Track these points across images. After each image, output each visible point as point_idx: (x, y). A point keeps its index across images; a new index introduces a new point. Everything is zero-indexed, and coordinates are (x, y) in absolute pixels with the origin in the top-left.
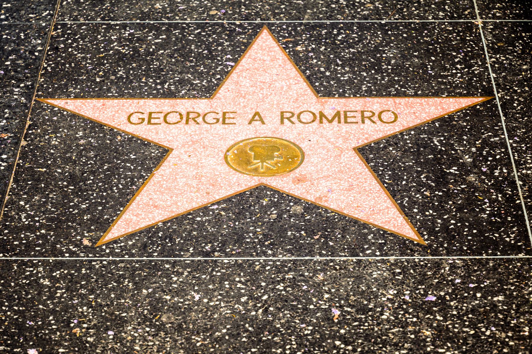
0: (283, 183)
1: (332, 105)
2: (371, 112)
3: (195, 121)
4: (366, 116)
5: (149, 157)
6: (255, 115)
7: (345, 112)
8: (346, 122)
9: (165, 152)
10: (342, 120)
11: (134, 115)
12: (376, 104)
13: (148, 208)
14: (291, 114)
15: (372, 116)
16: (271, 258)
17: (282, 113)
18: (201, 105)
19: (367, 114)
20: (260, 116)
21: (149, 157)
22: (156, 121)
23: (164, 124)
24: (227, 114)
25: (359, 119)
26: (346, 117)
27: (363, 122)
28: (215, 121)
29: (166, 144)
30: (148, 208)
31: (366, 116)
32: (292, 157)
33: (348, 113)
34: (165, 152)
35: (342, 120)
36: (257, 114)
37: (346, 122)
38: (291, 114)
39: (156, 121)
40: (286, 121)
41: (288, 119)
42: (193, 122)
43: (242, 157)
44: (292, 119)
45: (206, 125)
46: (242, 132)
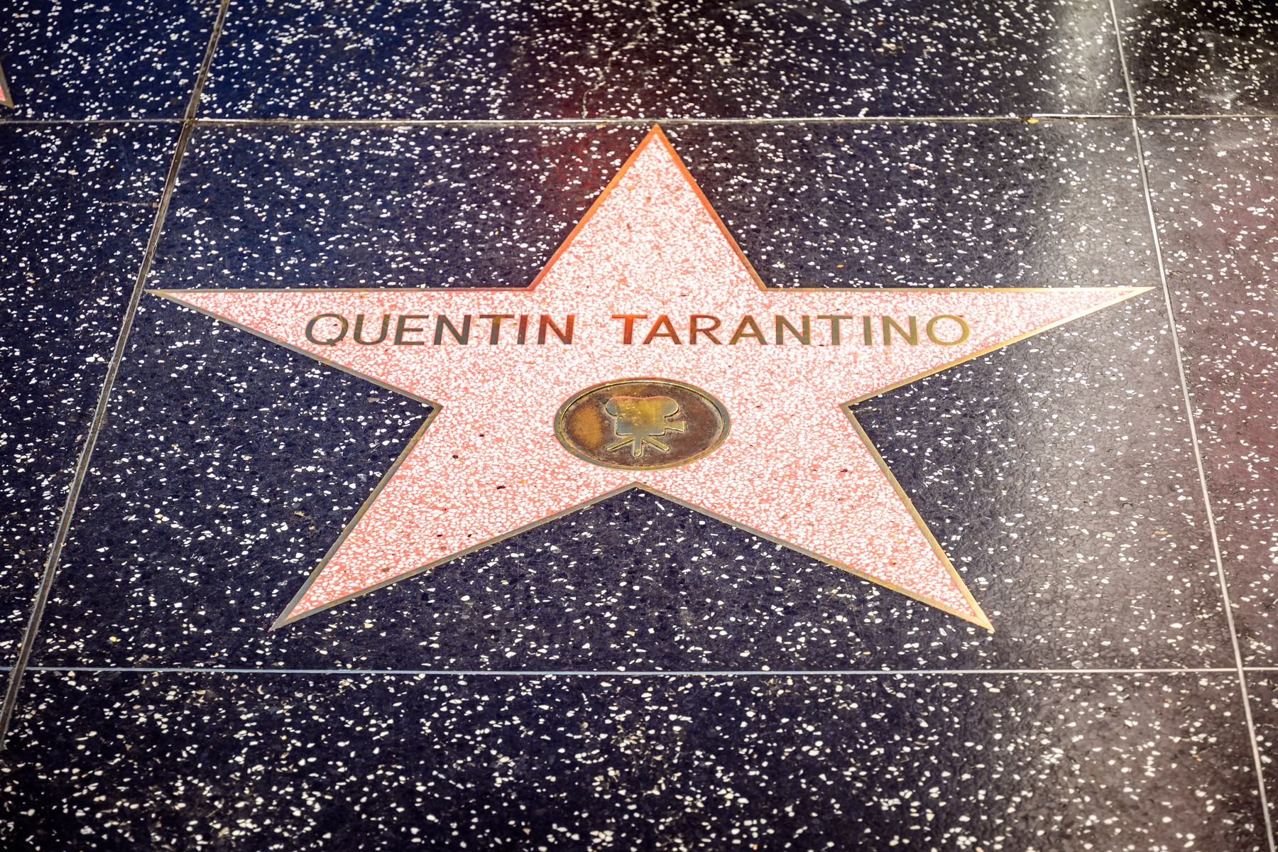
0: (684, 484)
2: (712, 318)
3: (709, 336)
4: (699, 327)
5: (377, 426)
6: (742, 326)
8: (398, 341)
9: (422, 412)
11: (319, 323)
13: (392, 538)
14: (712, 323)
15: (713, 328)
16: (946, 671)
17: (694, 319)
19: (704, 324)
20: (754, 327)
21: (377, 426)
22: (414, 337)
24: (408, 321)
25: (429, 334)
26: (401, 330)
30: (392, 538)
31: (699, 327)
32: (700, 424)
34: (422, 412)
36: (748, 320)
37: (398, 341)
38: (712, 323)
39: (414, 337)
40: (701, 338)
41: (707, 332)
43: (587, 422)
44: (714, 333)
45: (933, 347)
46: (600, 360)
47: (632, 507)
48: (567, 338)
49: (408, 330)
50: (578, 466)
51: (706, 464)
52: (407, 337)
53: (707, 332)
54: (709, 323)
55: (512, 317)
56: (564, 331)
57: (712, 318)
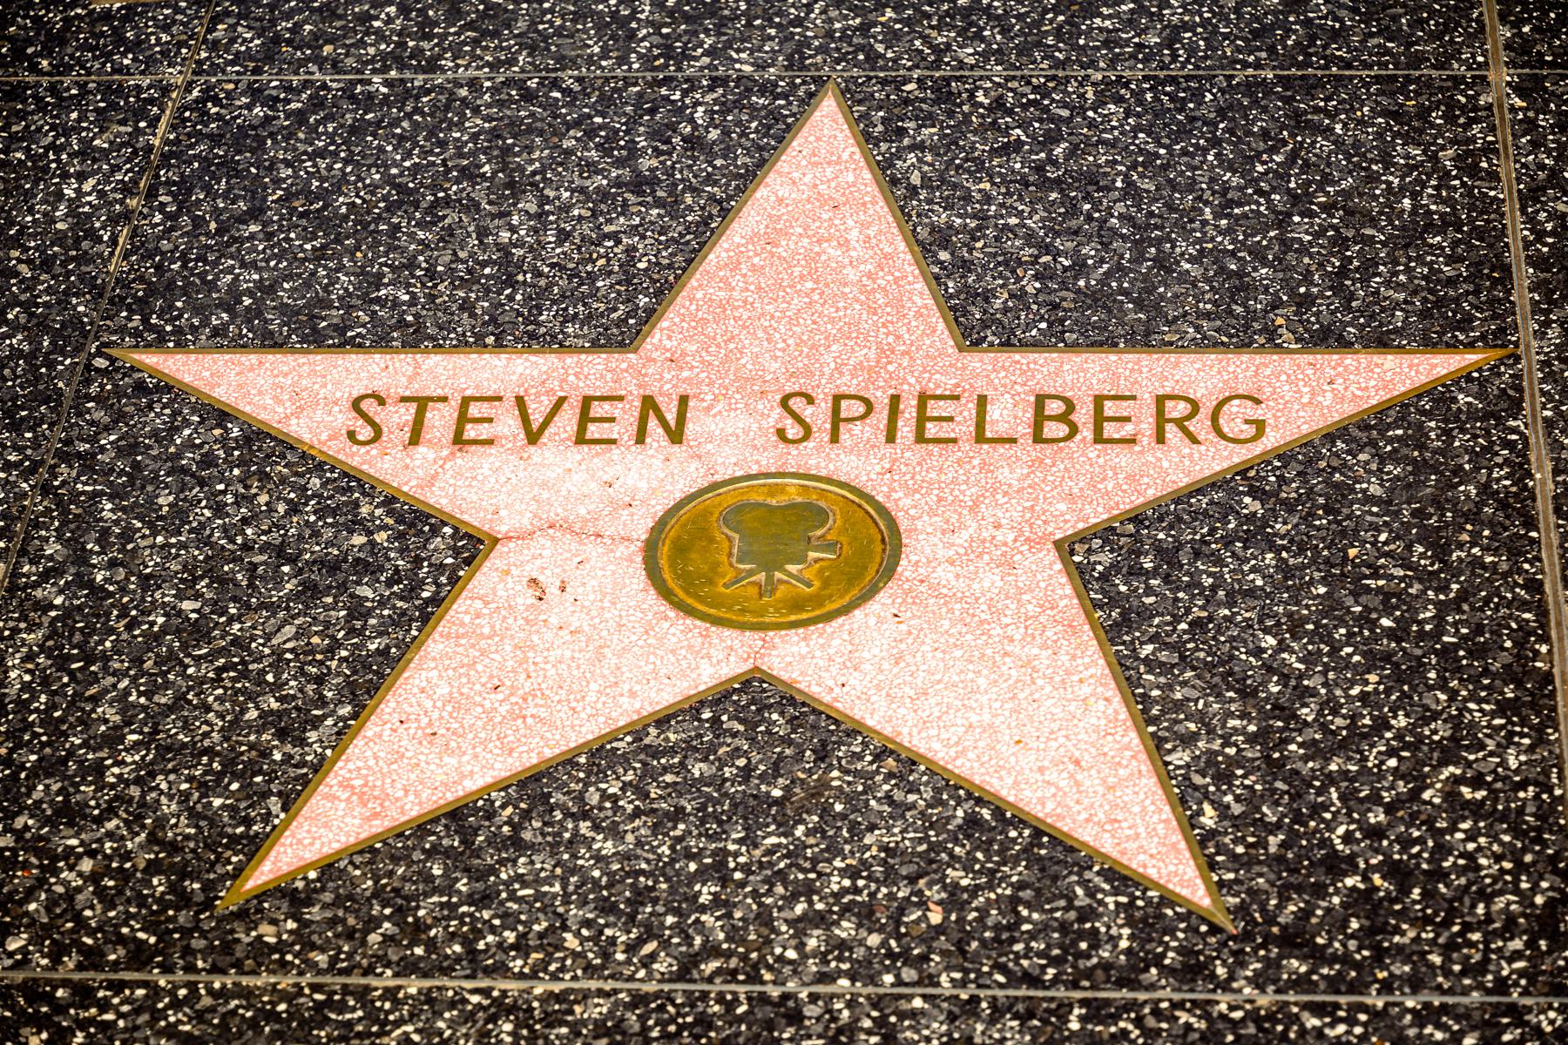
1: (1012, 379)
2: (1187, 399)
5: (427, 560)
7: (923, 399)
9: (472, 547)
10: (906, 430)
12: (1201, 374)
13: (417, 751)
17: (1041, 400)
18: (590, 371)
19: (1177, 409)
21: (427, 560)
22: (484, 431)
23: (1026, 446)
25: (1147, 425)
26: (1099, 419)
27: (1160, 438)
28: (1250, 431)
29: (474, 518)
30: (417, 751)
33: (1108, 404)
34: (472, 547)
35: (906, 430)
37: (1099, 438)
39: (945, 430)
40: (1171, 431)
41: (1180, 423)
42: (1175, 429)
44: (1191, 426)
47: (752, 697)
48: (676, 435)
49: (595, 420)
50: (678, 630)
51: (872, 622)
52: (471, 432)
53: (1180, 423)
54: (1181, 409)
55: (444, 399)
56: (535, 426)
57: (1187, 399)
